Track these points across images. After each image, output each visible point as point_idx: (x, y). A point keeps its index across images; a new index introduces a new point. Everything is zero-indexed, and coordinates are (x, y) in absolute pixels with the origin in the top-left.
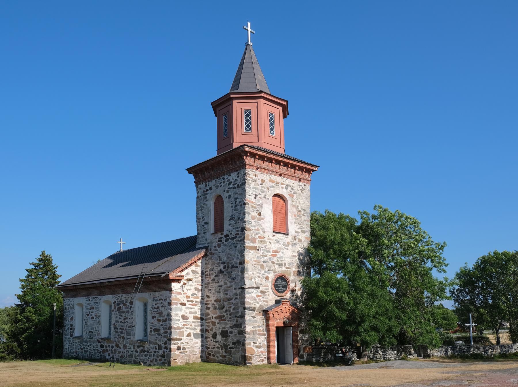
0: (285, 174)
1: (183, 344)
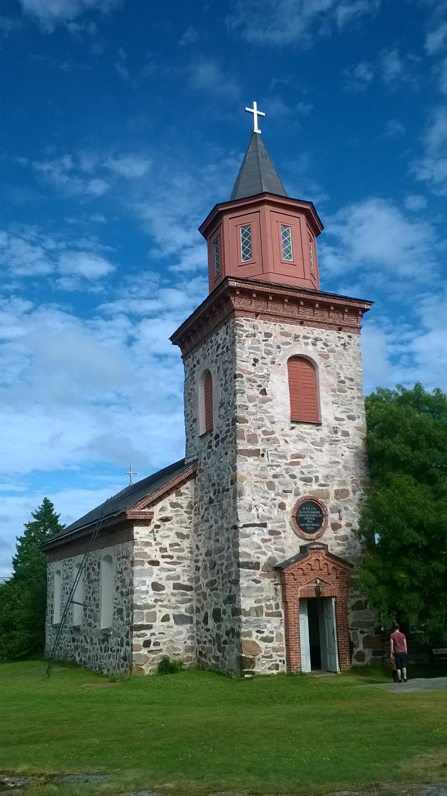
0: (310, 321)
1: (154, 636)
